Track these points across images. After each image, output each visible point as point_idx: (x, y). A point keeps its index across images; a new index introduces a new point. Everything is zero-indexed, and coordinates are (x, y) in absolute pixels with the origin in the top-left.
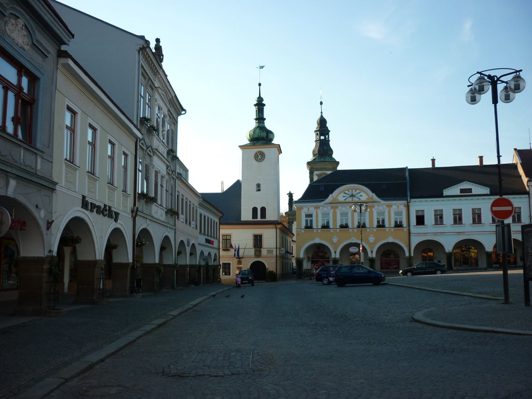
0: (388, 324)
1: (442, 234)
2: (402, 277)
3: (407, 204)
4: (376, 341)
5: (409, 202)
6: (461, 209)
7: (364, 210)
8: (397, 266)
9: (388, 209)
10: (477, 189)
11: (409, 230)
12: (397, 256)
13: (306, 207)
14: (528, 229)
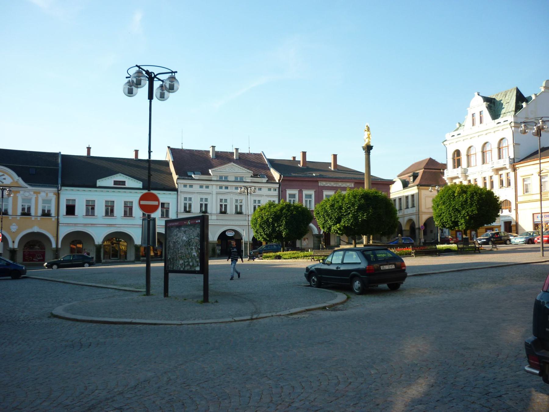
0: (23, 321)
1: (92, 225)
2: (47, 269)
3: (57, 192)
4: (6, 340)
5: (60, 190)
6: (114, 201)
7: (7, 195)
8: (42, 258)
9: (35, 196)
10: (130, 182)
11: (58, 219)
12: (43, 247)
13: (45, 192)
14: (171, 224)
